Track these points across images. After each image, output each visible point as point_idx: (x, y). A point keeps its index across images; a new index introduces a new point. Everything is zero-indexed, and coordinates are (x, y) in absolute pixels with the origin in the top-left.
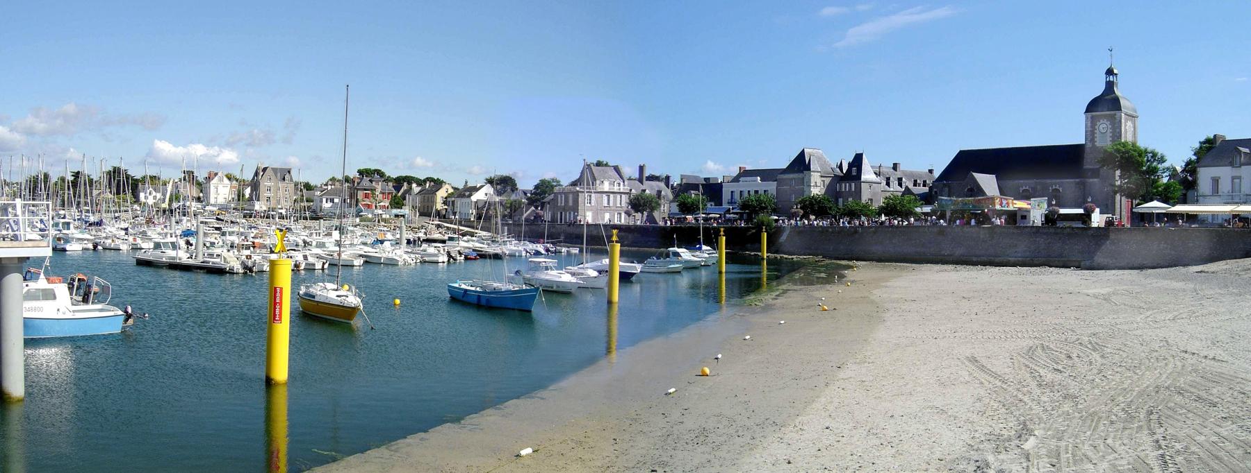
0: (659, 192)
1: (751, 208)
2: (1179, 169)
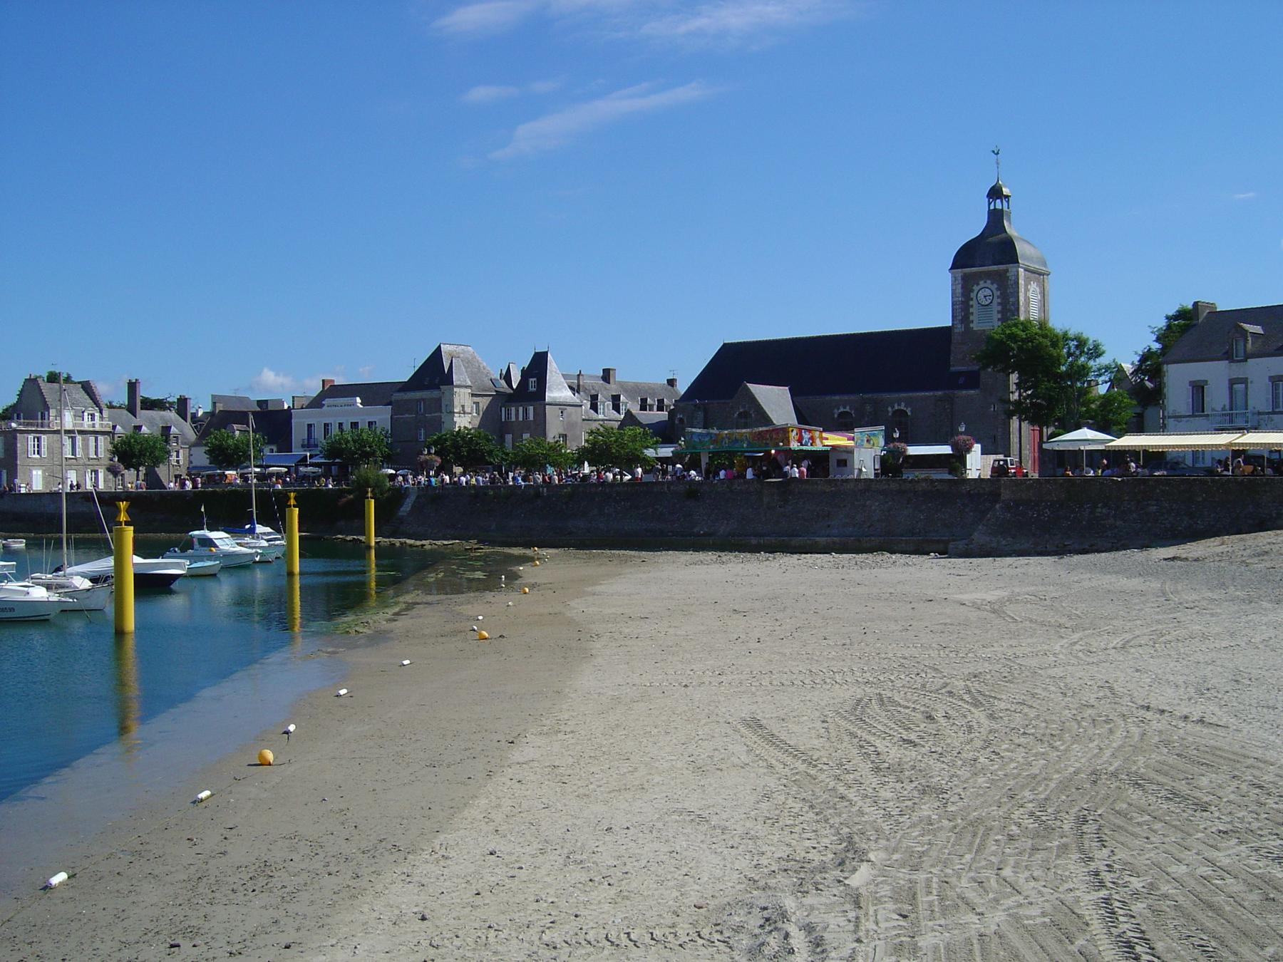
0: (166, 430)
1: (344, 455)
2: (1128, 368)
